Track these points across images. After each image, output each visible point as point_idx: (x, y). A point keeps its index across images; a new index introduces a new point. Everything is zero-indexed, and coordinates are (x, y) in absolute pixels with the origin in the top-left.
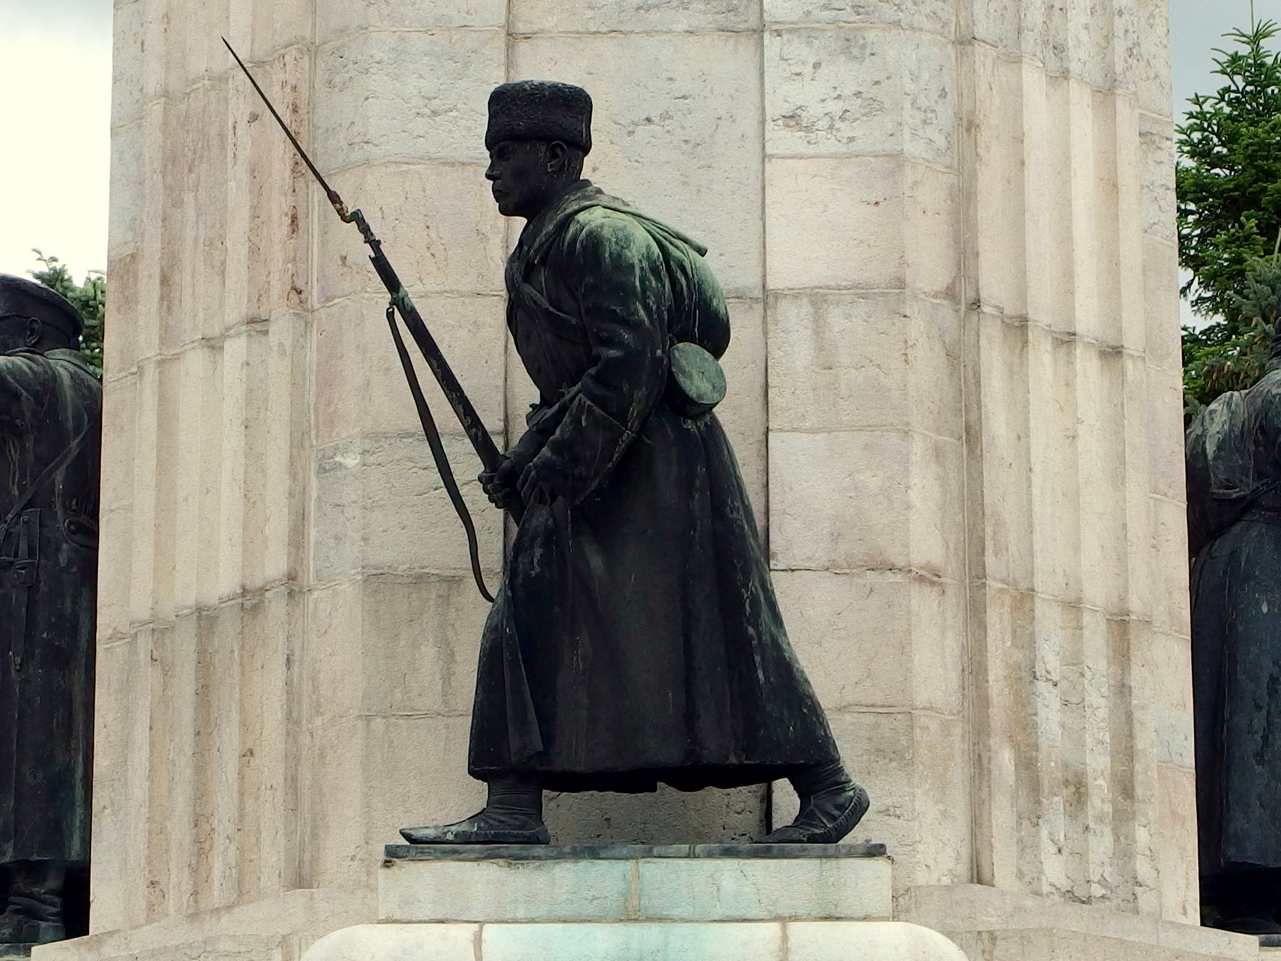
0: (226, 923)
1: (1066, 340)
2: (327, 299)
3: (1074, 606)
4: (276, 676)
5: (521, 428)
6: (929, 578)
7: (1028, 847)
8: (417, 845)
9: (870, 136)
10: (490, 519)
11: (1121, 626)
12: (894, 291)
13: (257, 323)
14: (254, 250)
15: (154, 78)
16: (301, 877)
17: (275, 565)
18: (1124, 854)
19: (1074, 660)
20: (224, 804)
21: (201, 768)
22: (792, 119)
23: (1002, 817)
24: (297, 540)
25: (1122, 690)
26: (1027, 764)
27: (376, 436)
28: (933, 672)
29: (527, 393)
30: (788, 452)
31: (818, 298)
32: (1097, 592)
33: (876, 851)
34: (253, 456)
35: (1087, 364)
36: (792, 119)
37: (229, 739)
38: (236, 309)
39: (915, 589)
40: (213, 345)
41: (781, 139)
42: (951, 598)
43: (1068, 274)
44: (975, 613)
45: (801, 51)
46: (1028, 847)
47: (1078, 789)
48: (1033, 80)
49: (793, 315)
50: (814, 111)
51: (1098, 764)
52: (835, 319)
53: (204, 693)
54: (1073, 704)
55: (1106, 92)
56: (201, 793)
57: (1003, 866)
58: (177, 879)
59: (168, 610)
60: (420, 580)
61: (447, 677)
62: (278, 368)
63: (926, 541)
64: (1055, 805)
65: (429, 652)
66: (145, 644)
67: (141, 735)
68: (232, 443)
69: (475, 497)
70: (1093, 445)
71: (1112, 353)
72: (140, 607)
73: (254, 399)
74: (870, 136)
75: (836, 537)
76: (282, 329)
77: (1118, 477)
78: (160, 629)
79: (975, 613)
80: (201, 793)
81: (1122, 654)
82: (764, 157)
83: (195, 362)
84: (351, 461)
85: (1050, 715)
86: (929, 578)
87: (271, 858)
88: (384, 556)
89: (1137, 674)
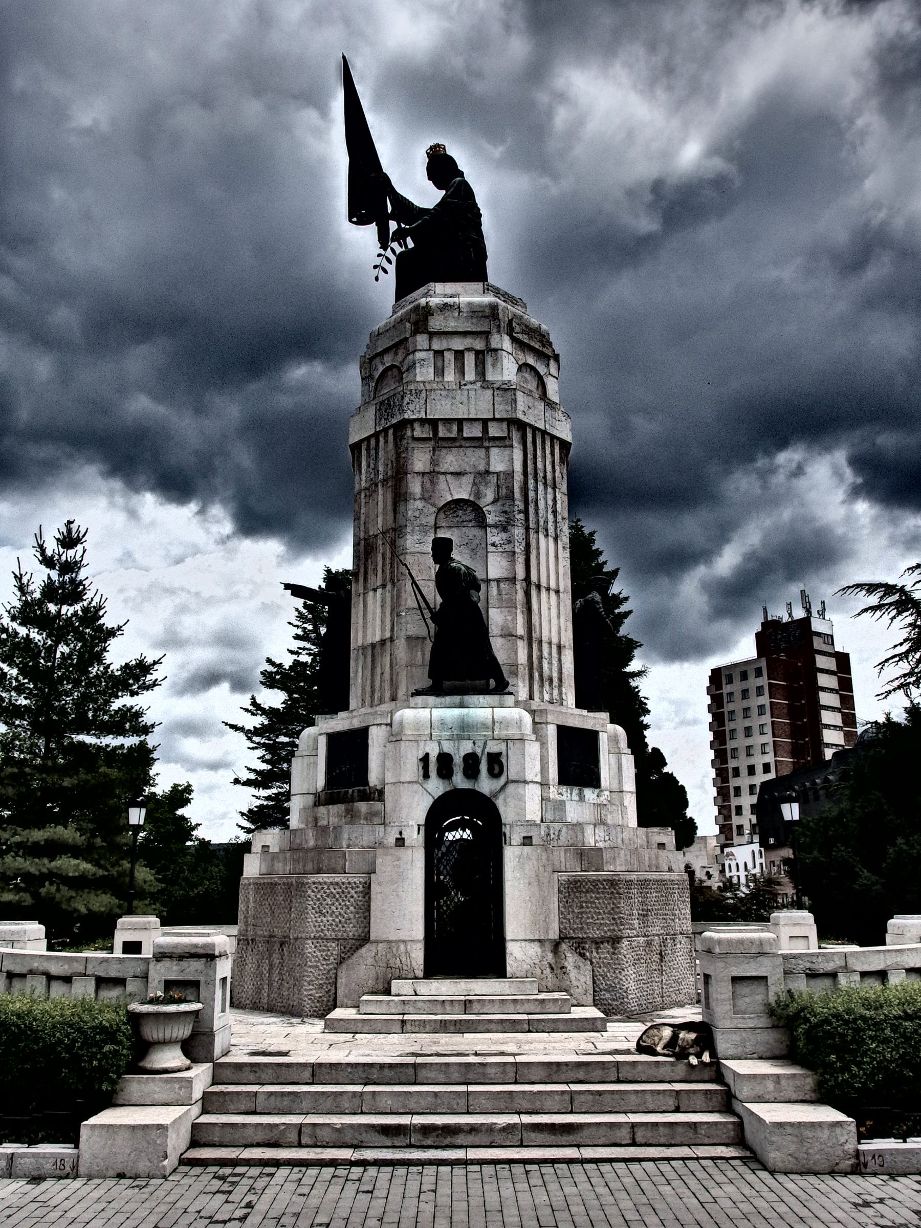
0: (378, 708)
1: (548, 589)
2: (398, 581)
3: (550, 643)
4: (389, 655)
5: (438, 607)
6: (521, 638)
7: (541, 692)
8: (418, 693)
9: (508, 547)
10: (432, 625)
11: (559, 647)
12: (513, 580)
13: (384, 586)
14: (383, 571)
15: (362, 535)
16: (394, 699)
17: (388, 635)
18: (560, 694)
19: (550, 654)
20: (377, 684)
21: (373, 675)
22: (493, 545)
23: (536, 687)
24: (392, 630)
25: (560, 660)
26: (541, 676)
27: (409, 609)
28: (522, 657)
29: (439, 600)
30: (492, 612)
31: (498, 581)
32: (555, 640)
33: (511, 694)
34: (383, 613)
35: (552, 594)
36: (493, 545)
37: (378, 671)
38: (379, 583)
39: (518, 640)
40: (375, 590)
41: (491, 548)
42: (526, 642)
43: (548, 576)
44: (527, 578)
45: (494, 530)
46: (541, 692)
47: (551, 680)
48: (541, 536)
49: (494, 585)
50: (497, 543)
51: (555, 675)
52: (502, 585)
53: (373, 661)
54: (550, 663)
55: (556, 539)
56: (373, 682)
57: (536, 695)
58: (368, 700)
59: (365, 644)
60: (418, 638)
61: (423, 658)
62: (389, 595)
63: (521, 630)
64: (546, 684)
65: (419, 653)
66: (361, 651)
67: (360, 670)
68: (379, 610)
69: (429, 621)
70: (554, 611)
71: (557, 592)
72: (360, 643)
73: (383, 601)
74: (508, 547)
75: (502, 630)
76: (389, 587)
77: (559, 617)
78: (364, 648)
79: (527, 578)
80: (373, 682)
81: (559, 653)
82: (487, 552)
83: (371, 593)
84: (403, 614)
85: (546, 666)
86: (521, 638)
87: (387, 695)
88: (410, 633)
89: (563, 657)
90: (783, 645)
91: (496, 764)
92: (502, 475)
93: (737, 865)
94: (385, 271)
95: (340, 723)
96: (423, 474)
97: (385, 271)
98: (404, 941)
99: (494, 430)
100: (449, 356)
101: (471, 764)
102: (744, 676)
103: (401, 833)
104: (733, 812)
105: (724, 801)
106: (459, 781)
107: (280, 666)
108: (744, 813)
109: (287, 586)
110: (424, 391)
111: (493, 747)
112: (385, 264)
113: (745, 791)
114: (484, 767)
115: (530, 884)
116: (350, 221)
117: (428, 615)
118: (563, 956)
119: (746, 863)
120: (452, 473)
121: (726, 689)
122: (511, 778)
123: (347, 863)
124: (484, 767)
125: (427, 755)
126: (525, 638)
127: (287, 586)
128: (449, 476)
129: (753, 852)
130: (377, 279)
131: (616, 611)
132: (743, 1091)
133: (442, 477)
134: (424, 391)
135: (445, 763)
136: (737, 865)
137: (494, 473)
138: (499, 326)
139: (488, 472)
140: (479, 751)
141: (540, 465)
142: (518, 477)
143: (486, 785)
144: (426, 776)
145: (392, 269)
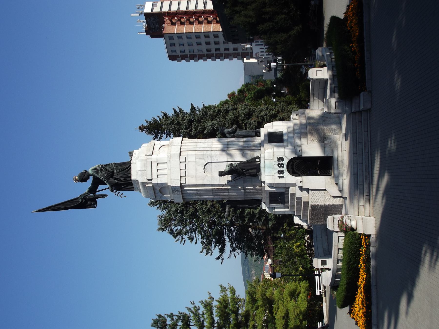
90: (157, 26)
91: (280, 159)
93: (261, 52)
94: (122, 194)
97: (122, 194)
98: (325, 180)
100: (160, 172)
101: (280, 165)
102: (173, 45)
104: (236, 52)
105: (231, 56)
106: (285, 168)
107: (203, 248)
108: (236, 47)
111: (276, 160)
112: (120, 194)
113: (226, 46)
114: (281, 162)
117: (239, 177)
119: (261, 48)
121: (178, 53)
124: (281, 162)
129: (256, 45)
130: (125, 196)
132: (358, 110)
133: (197, 174)
135: (280, 172)
136: (261, 52)
139: (196, 162)
142: (197, 153)
143: (285, 162)
144: (283, 177)
145: (121, 192)
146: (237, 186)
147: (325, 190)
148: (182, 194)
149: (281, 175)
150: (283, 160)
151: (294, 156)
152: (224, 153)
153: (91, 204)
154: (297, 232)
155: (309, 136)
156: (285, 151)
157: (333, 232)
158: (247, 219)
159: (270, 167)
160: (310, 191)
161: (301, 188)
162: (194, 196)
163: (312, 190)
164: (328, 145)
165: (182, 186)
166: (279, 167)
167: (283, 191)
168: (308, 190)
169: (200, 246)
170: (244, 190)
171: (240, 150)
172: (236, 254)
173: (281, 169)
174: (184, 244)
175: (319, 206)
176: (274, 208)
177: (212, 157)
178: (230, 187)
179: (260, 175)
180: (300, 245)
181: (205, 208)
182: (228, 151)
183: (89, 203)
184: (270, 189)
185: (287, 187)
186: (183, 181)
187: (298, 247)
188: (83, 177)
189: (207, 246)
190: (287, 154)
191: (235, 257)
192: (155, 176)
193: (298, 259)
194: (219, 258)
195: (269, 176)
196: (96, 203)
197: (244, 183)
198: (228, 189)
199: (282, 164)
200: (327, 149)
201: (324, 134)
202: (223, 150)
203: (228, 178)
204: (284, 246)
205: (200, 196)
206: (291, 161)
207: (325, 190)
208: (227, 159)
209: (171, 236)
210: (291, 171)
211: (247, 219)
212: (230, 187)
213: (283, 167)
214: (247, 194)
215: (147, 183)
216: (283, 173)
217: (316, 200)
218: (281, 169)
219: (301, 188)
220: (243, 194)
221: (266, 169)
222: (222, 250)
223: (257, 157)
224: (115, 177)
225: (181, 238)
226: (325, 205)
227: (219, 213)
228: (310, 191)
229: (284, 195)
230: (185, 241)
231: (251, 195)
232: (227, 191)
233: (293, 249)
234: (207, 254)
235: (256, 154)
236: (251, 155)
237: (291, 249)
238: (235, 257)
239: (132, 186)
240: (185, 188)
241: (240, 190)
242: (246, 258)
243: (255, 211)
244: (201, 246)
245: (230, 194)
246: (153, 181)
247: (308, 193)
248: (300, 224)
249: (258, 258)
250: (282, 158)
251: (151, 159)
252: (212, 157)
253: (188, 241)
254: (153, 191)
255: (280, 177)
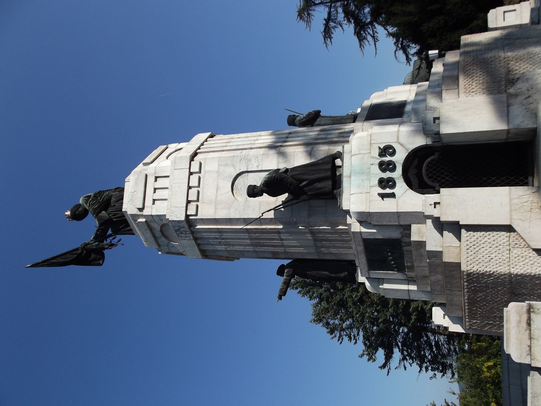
45: (250, 167)
50: (257, 164)
72: (313, 250)
92: (220, 163)
95: (361, 262)
96: (216, 208)
98: (511, 200)
99: (195, 167)
100: (157, 196)
101: (386, 166)
103: (430, 205)
109: (280, 298)
110: (171, 209)
111: (377, 152)
114: (388, 158)
115: (466, 116)
116: (102, 265)
117: (295, 201)
118: (520, 90)
120: (217, 192)
122: (396, 141)
123: (453, 245)
124: (388, 158)
125: (380, 195)
126: (313, 146)
127: (280, 298)
128: (218, 194)
131: (381, 287)
133: (218, 198)
134: (171, 209)
135: (384, 183)
137: (219, 168)
138: (144, 170)
139: (218, 172)
140: (378, 161)
141: (219, 145)
143: (399, 158)
144: (393, 195)
146: (296, 224)
147: (509, 229)
148: (196, 239)
149: (388, 191)
150: (393, 153)
151: (420, 141)
152: (272, 152)
153: (95, 260)
154: (491, 344)
155: (462, 81)
156: (398, 131)
157: (527, 369)
158: (413, 317)
159: (361, 173)
160: (463, 231)
161: (441, 226)
162: (216, 245)
163: (471, 228)
164: (519, 99)
165: (189, 222)
166: (383, 170)
167: (395, 234)
168: (456, 228)
169: (360, 346)
170: (312, 233)
171: (306, 144)
172: (407, 365)
173: (387, 175)
174: (341, 343)
175: (490, 275)
176: (382, 281)
177: (248, 160)
178: (281, 227)
179: (340, 194)
180: (495, 365)
181: (356, 297)
182: (282, 149)
183: (93, 256)
184: (364, 230)
185: (403, 222)
186: (192, 211)
187: (489, 368)
188: (78, 214)
189: (371, 350)
190: (404, 138)
191: (405, 368)
192: (148, 202)
193: (489, 388)
194: (384, 366)
195: (359, 196)
196: (103, 257)
197: (309, 216)
198: (278, 232)
199: (390, 163)
200: (516, 110)
201: (509, 72)
202: (271, 147)
203: (268, 203)
204: (468, 364)
205: (229, 245)
206: (415, 157)
207: (509, 229)
208: (278, 163)
209: (325, 330)
210: (415, 181)
211: (413, 317)
212: (281, 227)
213: (393, 169)
214: (319, 244)
215: (139, 216)
216: (393, 186)
217: (479, 256)
218: (387, 175)
219: (441, 226)
220: (311, 243)
221: (353, 178)
222: (388, 356)
223: (339, 155)
224: (110, 210)
225: (338, 335)
226: (510, 274)
227: (375, 306)
228: (463, 231)
229: (401, 247)
230: (342, 339)
231: (330, 247)
232: (276, 236)
233: (482, 370)
234: (369, 360)
235: (338, 148)
236: (324, 150)
237: (480, 371)
238: (405, 368)
239: (128, 228)
240: (198, 227)
241: (301, 233)
242: (420, 372)
243: (425, 307)
244: (363, 347)
245: (285, 243)
246: (146, 212)
247: (459, 237)
248: (446, 328)
249: (435, 374)
250: (390, 147)
251: (147, 170)
252: (248, 160)
253: (346, 339)
254: (148, 231)
255: (383, 196)
